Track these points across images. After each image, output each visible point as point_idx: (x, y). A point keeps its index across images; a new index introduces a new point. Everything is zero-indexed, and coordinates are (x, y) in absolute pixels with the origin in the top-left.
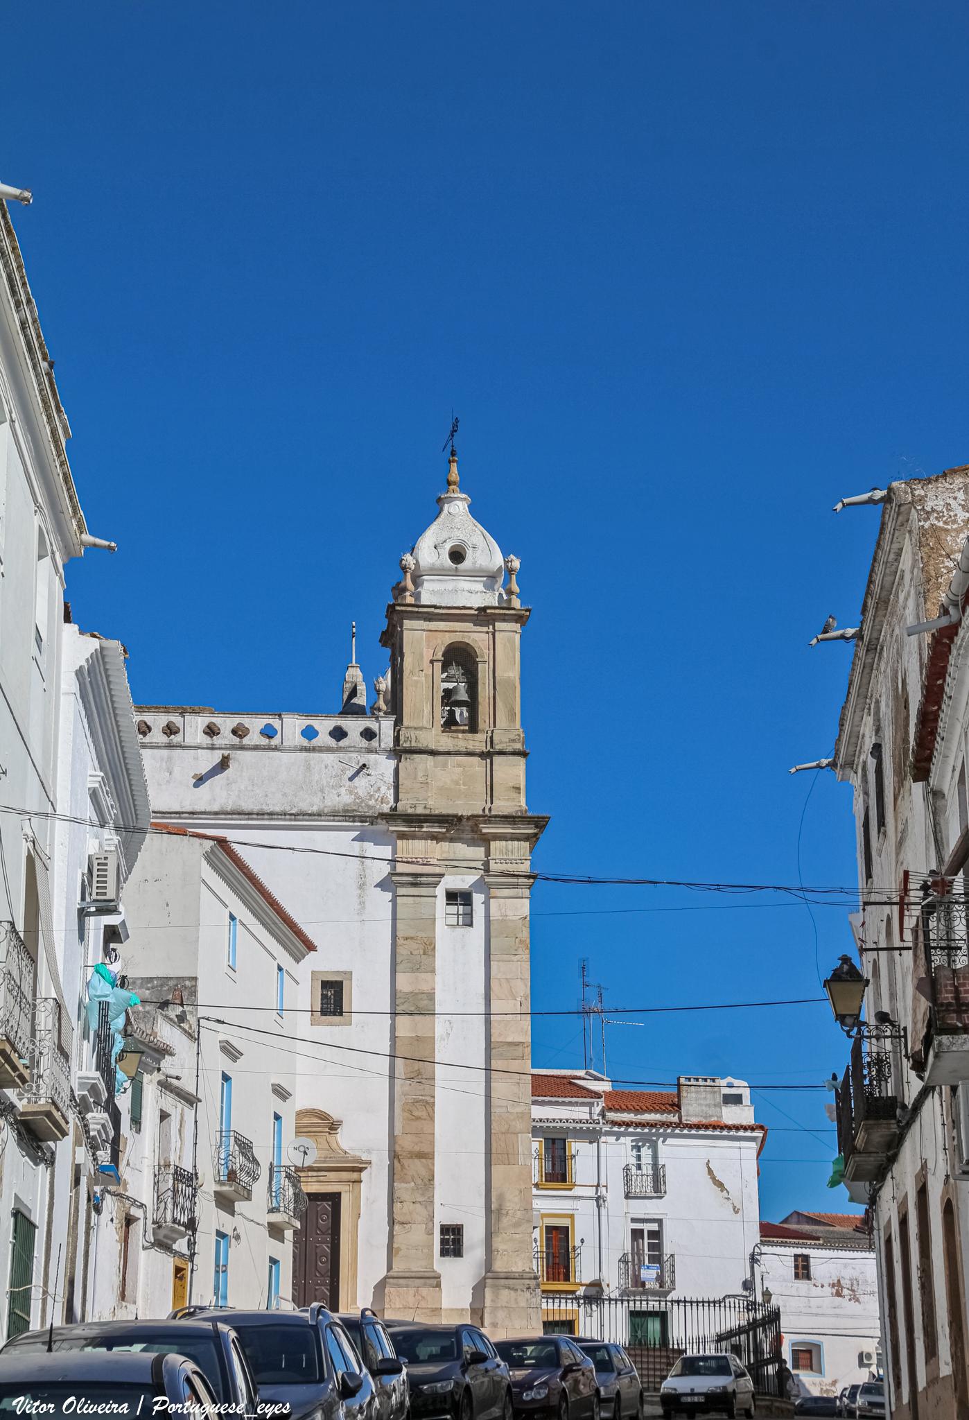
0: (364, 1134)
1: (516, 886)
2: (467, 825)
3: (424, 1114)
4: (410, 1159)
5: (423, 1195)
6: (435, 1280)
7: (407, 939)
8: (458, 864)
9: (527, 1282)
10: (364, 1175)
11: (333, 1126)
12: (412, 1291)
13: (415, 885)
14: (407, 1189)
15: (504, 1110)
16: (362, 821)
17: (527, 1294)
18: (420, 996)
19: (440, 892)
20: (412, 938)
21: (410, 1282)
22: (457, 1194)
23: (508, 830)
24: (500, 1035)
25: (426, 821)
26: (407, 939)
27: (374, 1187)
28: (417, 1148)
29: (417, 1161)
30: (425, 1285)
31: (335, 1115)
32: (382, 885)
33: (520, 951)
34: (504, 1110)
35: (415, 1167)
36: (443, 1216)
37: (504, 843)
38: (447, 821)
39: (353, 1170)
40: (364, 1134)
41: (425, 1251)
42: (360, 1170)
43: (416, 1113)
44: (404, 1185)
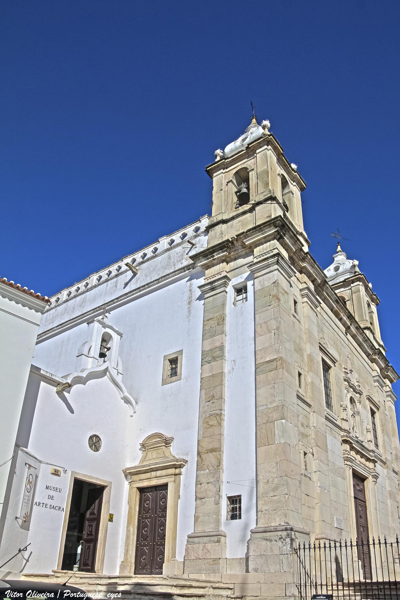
0: (185, 446)
1: (268, 266)
2: (237, 244)
3: (215, 423)
4: (210, 452)
5: (213, 477)
6: (218, 537)
7: (209, 320)
8: (238, 270)
9: (280, 533)
10: (183, 470)
11: (167, 442)
12: (201, 546)
13: (213, 289)
14: (204, 474)
15: (265, 407)
16: (188, 270)
17: (280, 544)
18: (214, 351)
19: (230, 289)
20: (211, 319)
21: (199, 535)
22: (237, 474)
23: (260, 236)
24: (262, 358)
25: (214, 252)
26: (209, 320)
27: (189, 474)
28: (210, 447)
29: (210, 455)
30: (210, 541)
31: (167, 434)
32: (200, 298)
33: (273, 302)
34: (265, 407)
35: (210, 458)
36: (227, 491)
37: (261, 246)
38: (224, 247)
39: (175, 467)
40: (185, 446)
41: (214, 516)
42: (181, 466)
43: (211, 423)
44: (202, 472)
